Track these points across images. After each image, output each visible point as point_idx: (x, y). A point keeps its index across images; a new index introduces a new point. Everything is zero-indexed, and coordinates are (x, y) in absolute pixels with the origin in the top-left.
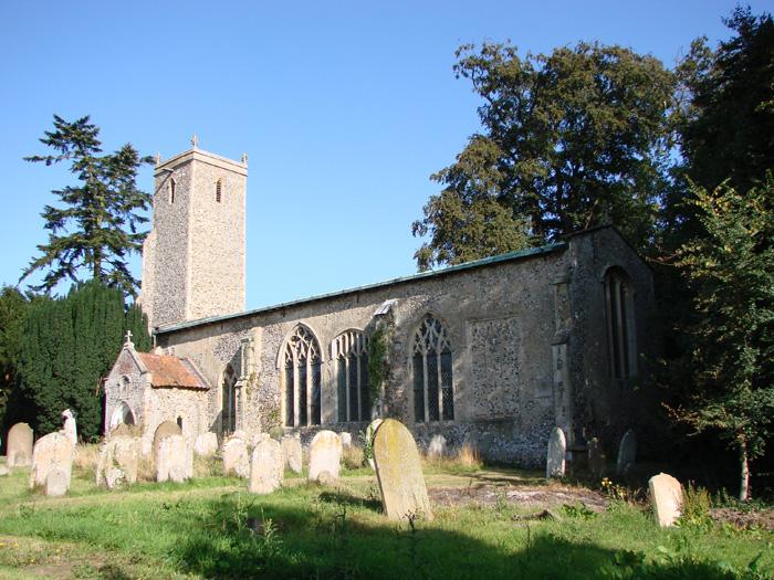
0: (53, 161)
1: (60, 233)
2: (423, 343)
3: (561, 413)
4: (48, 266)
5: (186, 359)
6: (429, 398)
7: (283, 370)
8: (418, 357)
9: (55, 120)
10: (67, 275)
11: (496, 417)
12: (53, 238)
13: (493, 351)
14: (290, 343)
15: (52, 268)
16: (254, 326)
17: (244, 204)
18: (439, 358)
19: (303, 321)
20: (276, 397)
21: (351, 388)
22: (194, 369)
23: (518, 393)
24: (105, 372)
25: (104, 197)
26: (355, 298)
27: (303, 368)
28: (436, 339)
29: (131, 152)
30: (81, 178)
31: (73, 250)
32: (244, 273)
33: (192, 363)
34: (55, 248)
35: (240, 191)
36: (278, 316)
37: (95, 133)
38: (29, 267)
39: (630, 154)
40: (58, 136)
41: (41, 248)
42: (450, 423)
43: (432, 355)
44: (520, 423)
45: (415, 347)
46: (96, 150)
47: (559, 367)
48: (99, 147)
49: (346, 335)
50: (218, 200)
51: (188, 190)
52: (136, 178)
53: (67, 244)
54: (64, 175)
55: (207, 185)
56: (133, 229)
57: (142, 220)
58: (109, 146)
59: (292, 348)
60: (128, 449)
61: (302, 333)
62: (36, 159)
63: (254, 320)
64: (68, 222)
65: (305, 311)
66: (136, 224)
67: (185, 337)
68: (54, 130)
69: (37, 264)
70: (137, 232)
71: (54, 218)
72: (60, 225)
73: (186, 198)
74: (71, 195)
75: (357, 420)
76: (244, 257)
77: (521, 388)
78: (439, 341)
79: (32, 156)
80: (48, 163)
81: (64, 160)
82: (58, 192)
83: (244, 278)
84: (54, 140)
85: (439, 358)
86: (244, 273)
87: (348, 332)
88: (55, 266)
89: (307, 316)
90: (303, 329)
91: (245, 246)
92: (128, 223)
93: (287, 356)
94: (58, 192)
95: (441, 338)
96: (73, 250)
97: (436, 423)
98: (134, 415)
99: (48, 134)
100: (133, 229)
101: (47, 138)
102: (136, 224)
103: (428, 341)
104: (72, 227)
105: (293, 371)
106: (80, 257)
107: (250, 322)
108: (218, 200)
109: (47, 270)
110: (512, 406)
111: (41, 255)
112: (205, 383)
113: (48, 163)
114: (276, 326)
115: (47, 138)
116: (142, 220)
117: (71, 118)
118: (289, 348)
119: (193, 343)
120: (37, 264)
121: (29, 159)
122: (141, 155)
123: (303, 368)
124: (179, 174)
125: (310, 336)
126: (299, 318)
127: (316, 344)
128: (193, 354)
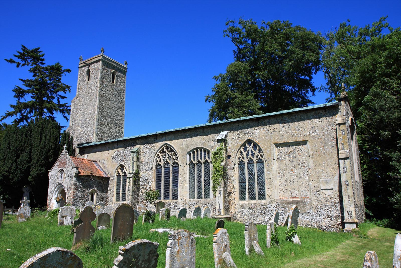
0: (20, 65)
1: (22, 100)
2: (244, 154)
3: (347, 199)
4: (14, 116)
6: (164, 185)
8: (241, 163)
9: (22, 47)
10: (25, 121)
11: (294, 199)
12: (19, 102)
13: (291, 162)
14: (160, 154)
15: (17, 117)
18: (246, 165)
19: (167, 142)
21: (165, 177)
22: (101, 168)
23: (308, 186)
24: (50, 166)
25: (46, 88)
26: (201, 130)
28: (253, 154)
29: (59, 66)
30: (34, 76)
31: (28, 109)
33: (99, 164)
34: (19, 108)
36: (153, 139)
37: (43, 56)
38: (5, 115)
39: (108, 140)
40: (24, 55)
41: (12, 106)
42: (263, 202)
43: (251, 162)
44: (310, 203)
45: (239, 158)
46: (43, 64)
47: (345, 172)
48: (44, 62)
49: (191, 153)
52: (62, 78)
53: (26, 106)
54: (26, 72)
56: (59, 101)
57: (63, 98)
58: (49, 62)
60: (147, 257)
62: (11, 61)
63: (138, 141)
64: (26, 95)
65: (170, 137)
66: (60, 99)
67: (95, 149)
68: (22, 51)
69: (10, 114)
70: (60, 103)
71: (20, 93)
72: (22, 97)
74: (29, 83)
75: (199, 196)
77: (311, 183)
78: (255, 155)
79: (9, 59)
80: (18, 66)
81: (26, 66)
82: (22, 80)
84: (22, 56)
85: (246, 165)
87: (197, 149)
88: (18, 116)
89: (171, 140)
92: (56, 99)
94: (22, 80)
95: (256, 153)
96: (28, 109)
97: (253, 202)
98: (66, 192)
99: (18, 52)
100: (59, 101)
101: (18, 54)
102: (60, 99)
103: (247, 155)
104: (28, 98)
106: (31, 113)
107: (136, 142)
109: (14, 117)
110: (304, 193)
111: (12, 110)
112: (107, 175)
113: (18, 66)
114: (151, 145)
115: (18, 54)
116: (63, 98)
117: (30, 47)
119: (100, 153)
120: (10, 114)
121: (7, 61)
122: (63, 69)
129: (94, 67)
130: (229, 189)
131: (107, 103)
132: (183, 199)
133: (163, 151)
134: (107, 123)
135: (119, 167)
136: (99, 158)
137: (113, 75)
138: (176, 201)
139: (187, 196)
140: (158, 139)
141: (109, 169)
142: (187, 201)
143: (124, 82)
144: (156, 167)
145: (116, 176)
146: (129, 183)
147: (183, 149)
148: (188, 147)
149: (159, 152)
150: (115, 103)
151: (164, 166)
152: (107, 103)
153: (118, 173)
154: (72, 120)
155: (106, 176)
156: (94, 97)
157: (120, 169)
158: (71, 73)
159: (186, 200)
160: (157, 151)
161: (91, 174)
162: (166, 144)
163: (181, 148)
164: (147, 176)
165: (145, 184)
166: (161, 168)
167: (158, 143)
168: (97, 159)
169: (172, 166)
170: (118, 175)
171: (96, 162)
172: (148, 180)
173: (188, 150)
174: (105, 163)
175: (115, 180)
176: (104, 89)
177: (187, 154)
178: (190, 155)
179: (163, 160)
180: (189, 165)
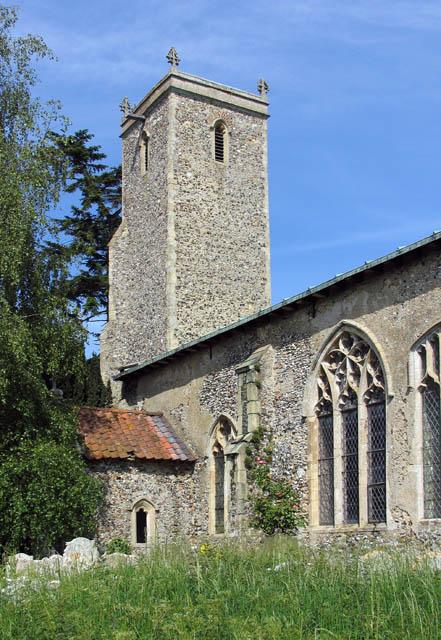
5: (161, 415)
7: (313, 419)
8: (325, 407)
9: (100, 152)
14: (326, 365)
16: (262, 344)
17: (265, 162)
20: (301, 472)
27: (350, 415)
32: (268, 276)
33: (171, 422)
35: (256, 142)
36: (303, 317)
50: (219, 156)
51: (165, 143)
55: (198, 132)
59: (330, 376)
61: (348, 344)
73: (163, 157)
76: (267, 251)
83: (268, 285)
86: (268, 276)
90: (351, 337)
91: (267, 233)
93: (320, 392)
105: (217, 505)
108: (219, 156)
118: (324, 378)
123: (350, 415)
124: (152, 121)
125: (365, 348)
126: (344, 316)
127: (376, 362)
128: (170, 405)
129: (155, 122)
130: (235, 480)
131: (203, 230)
132: (401, 520)
133: (335, 354)
134: (209, 293)
135: (219, 426)
136: (168, 402)
137: (218, 129)
138: (381, 526)
139: (415, 510)
140: (318, 315)
141: (194, 435)
142: (414, 528)
143: (258, 156)
144: (318, 413)
145: (211, 456)
146: (232, 475)
147: (396, 335)
148: (414, 325)
149: (325, 359)
150: (232, 226)
151: (341, 406)
152: (203, 230)
153: (218, 445)
154: (115, 301)
155: (184, 457)
156: (161, 217)
157: (222, 430)
158: (108, 157)
159: (411, 523)
160: (318, 358)
161: (132, 453)
162: (343, 325)
163: (390, 333)
164: (289, 448)
165: (285, 474)
166: (331, 415)
167: (322, 332)
168: (164, 408)
169: (367, 401)
170: (216, 450)
171: (161, 415)
172: (295, 461)
173: (416, 335)
174: (184, 417)
175: (212, 466)
176: (191, 185)
177: (412, 349)
178: (423, 354)
179: (339, 384)
180: (422, 390)
